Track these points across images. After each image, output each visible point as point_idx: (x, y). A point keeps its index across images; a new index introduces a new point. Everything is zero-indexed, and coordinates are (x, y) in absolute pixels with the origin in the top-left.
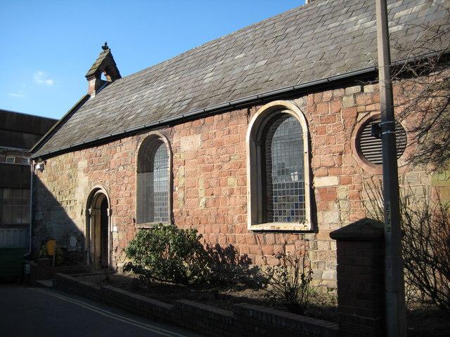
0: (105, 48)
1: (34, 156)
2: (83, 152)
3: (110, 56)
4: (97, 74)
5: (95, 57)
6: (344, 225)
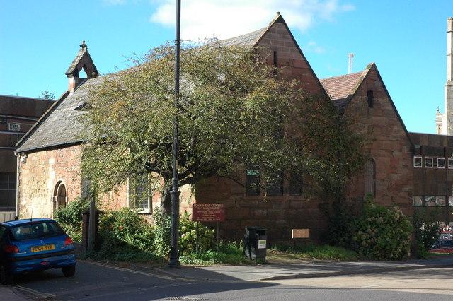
0: (83, 46)
1: (18, 150)
2: (52, 152)
3: (87, 54)
4: (75, 73)
5: (77, 54)
6: (441, 134)
